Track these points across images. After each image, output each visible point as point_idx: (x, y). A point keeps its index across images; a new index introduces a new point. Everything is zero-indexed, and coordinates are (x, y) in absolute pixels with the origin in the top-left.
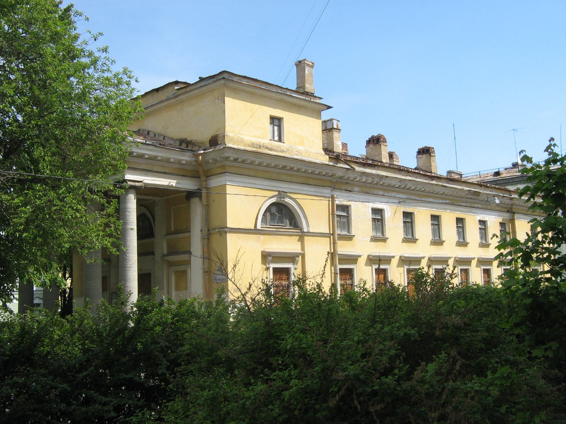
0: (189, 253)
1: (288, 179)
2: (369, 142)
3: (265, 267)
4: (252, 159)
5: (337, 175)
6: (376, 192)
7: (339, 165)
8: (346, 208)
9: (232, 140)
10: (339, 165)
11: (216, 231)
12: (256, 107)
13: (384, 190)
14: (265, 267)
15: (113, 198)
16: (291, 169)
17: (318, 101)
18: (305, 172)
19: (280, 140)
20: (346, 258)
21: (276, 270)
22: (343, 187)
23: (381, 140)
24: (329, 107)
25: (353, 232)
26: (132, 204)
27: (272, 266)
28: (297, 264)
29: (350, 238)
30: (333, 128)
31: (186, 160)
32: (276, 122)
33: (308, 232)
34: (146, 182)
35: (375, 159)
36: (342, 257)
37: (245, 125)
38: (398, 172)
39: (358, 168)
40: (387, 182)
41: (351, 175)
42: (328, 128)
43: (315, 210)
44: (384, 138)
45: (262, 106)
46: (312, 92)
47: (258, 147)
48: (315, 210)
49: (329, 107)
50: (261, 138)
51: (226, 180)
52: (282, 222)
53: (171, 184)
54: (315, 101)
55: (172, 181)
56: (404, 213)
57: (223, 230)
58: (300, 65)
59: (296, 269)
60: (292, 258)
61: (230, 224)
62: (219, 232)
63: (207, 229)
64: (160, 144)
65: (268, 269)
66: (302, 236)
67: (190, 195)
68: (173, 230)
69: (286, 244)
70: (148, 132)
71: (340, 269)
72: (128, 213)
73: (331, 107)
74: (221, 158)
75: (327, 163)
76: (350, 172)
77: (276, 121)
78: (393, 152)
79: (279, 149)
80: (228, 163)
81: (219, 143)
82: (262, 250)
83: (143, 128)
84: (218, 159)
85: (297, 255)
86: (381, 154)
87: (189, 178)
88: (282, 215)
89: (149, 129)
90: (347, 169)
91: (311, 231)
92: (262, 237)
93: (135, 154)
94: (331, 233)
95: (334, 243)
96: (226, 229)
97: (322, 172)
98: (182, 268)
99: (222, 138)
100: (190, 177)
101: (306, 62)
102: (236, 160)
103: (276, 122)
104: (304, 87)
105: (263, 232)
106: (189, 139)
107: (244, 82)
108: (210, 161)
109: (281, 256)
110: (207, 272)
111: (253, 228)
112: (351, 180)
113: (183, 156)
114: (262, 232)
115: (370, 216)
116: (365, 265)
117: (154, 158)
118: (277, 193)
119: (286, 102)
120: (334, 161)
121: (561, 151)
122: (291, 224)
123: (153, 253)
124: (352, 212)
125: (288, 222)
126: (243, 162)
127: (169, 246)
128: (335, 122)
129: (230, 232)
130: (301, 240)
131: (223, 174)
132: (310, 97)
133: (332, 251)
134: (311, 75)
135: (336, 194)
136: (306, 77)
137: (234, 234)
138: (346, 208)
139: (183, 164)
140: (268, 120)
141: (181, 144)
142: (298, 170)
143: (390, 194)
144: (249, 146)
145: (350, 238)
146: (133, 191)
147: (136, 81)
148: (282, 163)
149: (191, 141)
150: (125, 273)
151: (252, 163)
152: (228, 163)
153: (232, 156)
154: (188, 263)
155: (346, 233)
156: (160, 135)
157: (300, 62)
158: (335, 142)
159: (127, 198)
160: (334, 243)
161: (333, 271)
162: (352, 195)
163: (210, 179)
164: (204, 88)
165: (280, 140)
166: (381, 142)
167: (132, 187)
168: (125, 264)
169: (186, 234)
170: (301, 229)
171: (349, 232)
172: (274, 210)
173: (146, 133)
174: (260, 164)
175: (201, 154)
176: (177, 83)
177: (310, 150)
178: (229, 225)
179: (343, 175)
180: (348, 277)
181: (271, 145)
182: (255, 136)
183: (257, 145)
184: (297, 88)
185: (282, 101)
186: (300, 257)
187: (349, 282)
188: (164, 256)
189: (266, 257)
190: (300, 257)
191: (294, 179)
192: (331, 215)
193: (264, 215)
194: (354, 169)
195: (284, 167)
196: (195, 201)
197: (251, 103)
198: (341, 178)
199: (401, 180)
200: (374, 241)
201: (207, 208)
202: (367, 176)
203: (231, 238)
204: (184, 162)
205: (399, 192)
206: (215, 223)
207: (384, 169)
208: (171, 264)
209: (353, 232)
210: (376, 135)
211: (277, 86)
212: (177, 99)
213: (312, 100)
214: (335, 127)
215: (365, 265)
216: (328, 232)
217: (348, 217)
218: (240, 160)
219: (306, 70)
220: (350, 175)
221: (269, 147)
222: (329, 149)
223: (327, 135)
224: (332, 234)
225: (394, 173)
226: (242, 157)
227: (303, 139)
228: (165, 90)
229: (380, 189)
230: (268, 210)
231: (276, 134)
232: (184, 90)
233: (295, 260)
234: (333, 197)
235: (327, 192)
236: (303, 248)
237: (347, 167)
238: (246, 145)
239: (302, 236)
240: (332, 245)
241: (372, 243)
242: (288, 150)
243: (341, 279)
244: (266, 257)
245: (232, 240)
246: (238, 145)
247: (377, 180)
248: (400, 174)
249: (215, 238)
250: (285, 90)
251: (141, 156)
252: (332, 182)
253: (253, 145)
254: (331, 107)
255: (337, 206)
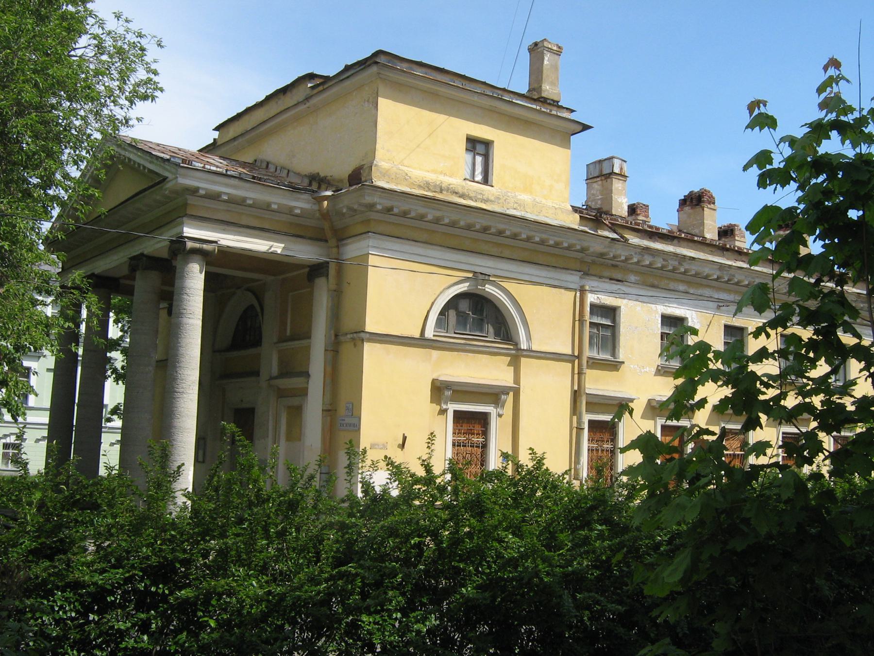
0: (307, 375)
1: (494, 251)
2: (683, 203)
3: (438, 408)
4: (422, 210)
5: (591, 250)
6: (672, 285)
7: (600, 232)
8: (611, 312)
9: (385, 174)
10: (600, 232)
11: (348, 338)
12: (440, 118)
13: (689, 283)
14: (438, 408)
15: (166, 269)
16: (500, 233)
17: (566, 115)
18: (568, 248)
19: (486, 181)
20: (602, 401)
21: (459, 417)
22: (607, 273)
23: (705, 199)
24: (586, 127)
25: (622, 356)
26: (195, 281)
27: (452, 407)
28: (503, 406)
29: (614, 366)
30: (613, 173)
31: (279, 204)
32: (480, 148)
33: (529, 350)
34: (223, 242)
35: (693, 232)
36: (596, 400)
37: (414, 149)
38: (720, 252)
39: (634, 240)
40: (694, 268)
41: (622, 252)
42: (604, 173)
43: (545, 311)
44: (711, 197)
45: (451, 118)
46: (556, 99)
47: (438, 190)
48: (545, 311)
49: (586, 127)
50: (445, 174)
51: (368, 246)
52: (481, 330)
53: (273, 249)
54: (559, 114)
55: (276, 244)
56: (727, 327)
57: (360, 336)
58: (536, 50)
59: (500, 416)
60: (494, 395)
61: (371, 326)
62: (353, 339)
63: (332, 332)
64: (254, 178)
65: (443, 412)
66: (516, 357)
67: (317, 270)
68: (288, 333)
69: (484, 369)
70: (268, 163)
71: (591, 422)
72: (185, 297)
73: (589, 127)
74: (360, 205)
75: (576, 227)
76: (618, 246)
77: (475, 145)
78: (735, 225)
79: (479, 197)
80: (374, 216)
81: (363, 179)
82: (435, 376)
83: (261, 157)
84: (356, 207)
85: (505, 390)
86: (703, 224)
87: (309, 241)
88: (478, 316)
89: (269, 159)
90: (613, 239)
91: (534, 349)
92: (435, 353)
93: (202, 192)
94: (576, 354)
95: (580, 373)
96: (362, 335)
97: (562, 243)
98: (295, 401)
99: (367, 171)
100: (311, 239)
101: (546, 44)
102: (389, 210)
103: (480, 148)
104: (539, 89)
105: (439, 345)
106: (322, 175)
107: (419, 72)
108: (350, 212)
109: (484, 390)
110: (329, 410)
111: (417, 335)
112: (623, 261)
113: (297, 200)
114: (434, 344)
115: (657, 328)
116: (642, 418)
117: (240, 202)
118: (470, 275)
119: (501, 114)
120: (591, 224)
121: (858, 97)
122: (497, 334)
123: (257, 374)
124: (622, 320)
125: (491, 330)
126: (404, 214)
127: (282, 362)
128: (617, 164)
129: (369, 340)
130: (515, 363)
131: (364, 236)
132: (550, 107)
133: (576, 388)
134: (555, 67)
135: (589, 284)
136: (545, 71)
137: (378, 345)
138: (611, 312)
139: (297, 216)
140: (463, 144)
141: (310, 184)
142: (515, 236)
143: (700, 292)
144: (420, 187)
145: (614, 366)
146: (198, 257)
147: (159, 45)
148: (480, 222)
149: (325, 177)
150: (172, 403)
151: (421, 218)
152: (374, 216)
153: (381, 203)
154: (303, 393)
155: (608, 357)
156: (283, 168)
157: (536, 44)
158: (615, 197)
159: (187, 269)
160: (580, 373)
161: (575, 424)
162: (624, 288)
163: (344, 245)
164: (347, 83)
165: (486, 181)
166: (704, 202)
167: (194, 251)
168: (173, 387)
169: (304, 342)
170: (516, 344)
171: (614, 354)
172: (464, 306)
173: (264, 166)
174: (437, 221)
175: (327, 198)
176: (311, 76)
177: (544, 201)
178: (369, 328)
179: (605, 250)
180: (606, 436)
181: (463, 187)
182: (434, 171)
183: (435, 186)
184: (529, 91)
185: (492, 111)
186: (511, 394)
187: (607, 446)
188: (271, 378)
189: (440, 390)
190: (511, 394)
191: (507, 253)
192: (577, 323)
193: (442, 313)
194: (627, 240)
195: (485, 230)
196: (321, 282)
197: (431, 110)
198: (602, 255)
199: (722, 266)
200: (662, 375)
201: (337, 295)
202: (653, 256)
203: (370, 351)
204: (298, 211)
205: (719, 289)
206: (348, 324)
207: (691, 244)
208: (282, 394)
209: (621, 356)
210: (696, 190)
211: (484, 83)
212: (308, 105)
213: (554, 112)
214: (617, 170)
215: (642, 418)
216: (570, 353)
217: (614, 329)
218: (396, 211)
219: (546, 58)
220: (618, 252)
221: (460, 191)
222: (605, 209)
223: (603, 186)
224: (578, 357)
225: (712, 253)
226: (400, 206)
227: (538, 182)
228: (295, 91)
229: (682, 281)
230: (453, 303)
231: (479, 169)
232: (321, 88)
233: (500, 399)
234: (583, 291)
235: (573, 279)
236: (517, 380)
237: (615, 236)
238: (412, 185)
239: (516, 357)
240: (576, 376)
241: (659, 378)
242: (499, 198)
243: (591, 440)
244: (440, 390)
245: (372, 355)
246: (397, 184)
247: (673, 263)
248: (723, 256)
249: (346, 349)
250: (500, 92)
251: (215, 197)
252: (582, 262)
253: (427, 185)
254: (589, 127)
255: (593, 306)
